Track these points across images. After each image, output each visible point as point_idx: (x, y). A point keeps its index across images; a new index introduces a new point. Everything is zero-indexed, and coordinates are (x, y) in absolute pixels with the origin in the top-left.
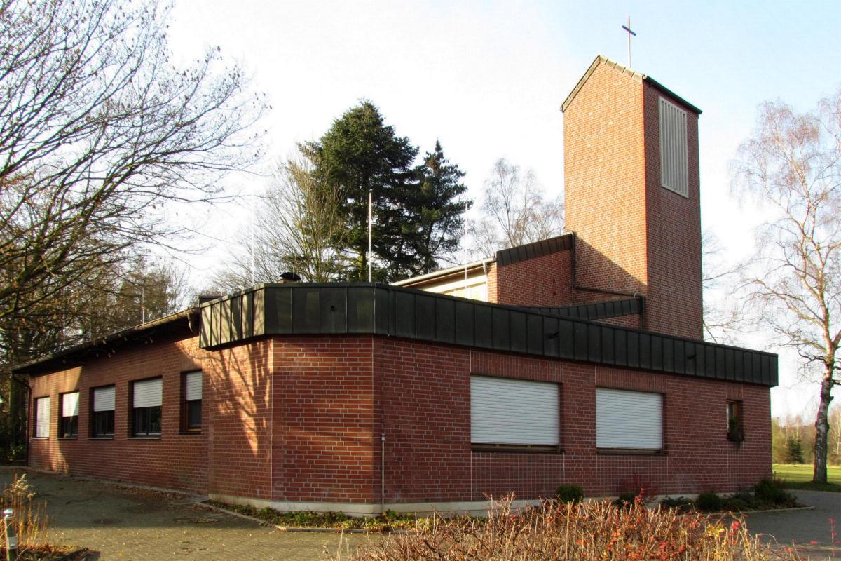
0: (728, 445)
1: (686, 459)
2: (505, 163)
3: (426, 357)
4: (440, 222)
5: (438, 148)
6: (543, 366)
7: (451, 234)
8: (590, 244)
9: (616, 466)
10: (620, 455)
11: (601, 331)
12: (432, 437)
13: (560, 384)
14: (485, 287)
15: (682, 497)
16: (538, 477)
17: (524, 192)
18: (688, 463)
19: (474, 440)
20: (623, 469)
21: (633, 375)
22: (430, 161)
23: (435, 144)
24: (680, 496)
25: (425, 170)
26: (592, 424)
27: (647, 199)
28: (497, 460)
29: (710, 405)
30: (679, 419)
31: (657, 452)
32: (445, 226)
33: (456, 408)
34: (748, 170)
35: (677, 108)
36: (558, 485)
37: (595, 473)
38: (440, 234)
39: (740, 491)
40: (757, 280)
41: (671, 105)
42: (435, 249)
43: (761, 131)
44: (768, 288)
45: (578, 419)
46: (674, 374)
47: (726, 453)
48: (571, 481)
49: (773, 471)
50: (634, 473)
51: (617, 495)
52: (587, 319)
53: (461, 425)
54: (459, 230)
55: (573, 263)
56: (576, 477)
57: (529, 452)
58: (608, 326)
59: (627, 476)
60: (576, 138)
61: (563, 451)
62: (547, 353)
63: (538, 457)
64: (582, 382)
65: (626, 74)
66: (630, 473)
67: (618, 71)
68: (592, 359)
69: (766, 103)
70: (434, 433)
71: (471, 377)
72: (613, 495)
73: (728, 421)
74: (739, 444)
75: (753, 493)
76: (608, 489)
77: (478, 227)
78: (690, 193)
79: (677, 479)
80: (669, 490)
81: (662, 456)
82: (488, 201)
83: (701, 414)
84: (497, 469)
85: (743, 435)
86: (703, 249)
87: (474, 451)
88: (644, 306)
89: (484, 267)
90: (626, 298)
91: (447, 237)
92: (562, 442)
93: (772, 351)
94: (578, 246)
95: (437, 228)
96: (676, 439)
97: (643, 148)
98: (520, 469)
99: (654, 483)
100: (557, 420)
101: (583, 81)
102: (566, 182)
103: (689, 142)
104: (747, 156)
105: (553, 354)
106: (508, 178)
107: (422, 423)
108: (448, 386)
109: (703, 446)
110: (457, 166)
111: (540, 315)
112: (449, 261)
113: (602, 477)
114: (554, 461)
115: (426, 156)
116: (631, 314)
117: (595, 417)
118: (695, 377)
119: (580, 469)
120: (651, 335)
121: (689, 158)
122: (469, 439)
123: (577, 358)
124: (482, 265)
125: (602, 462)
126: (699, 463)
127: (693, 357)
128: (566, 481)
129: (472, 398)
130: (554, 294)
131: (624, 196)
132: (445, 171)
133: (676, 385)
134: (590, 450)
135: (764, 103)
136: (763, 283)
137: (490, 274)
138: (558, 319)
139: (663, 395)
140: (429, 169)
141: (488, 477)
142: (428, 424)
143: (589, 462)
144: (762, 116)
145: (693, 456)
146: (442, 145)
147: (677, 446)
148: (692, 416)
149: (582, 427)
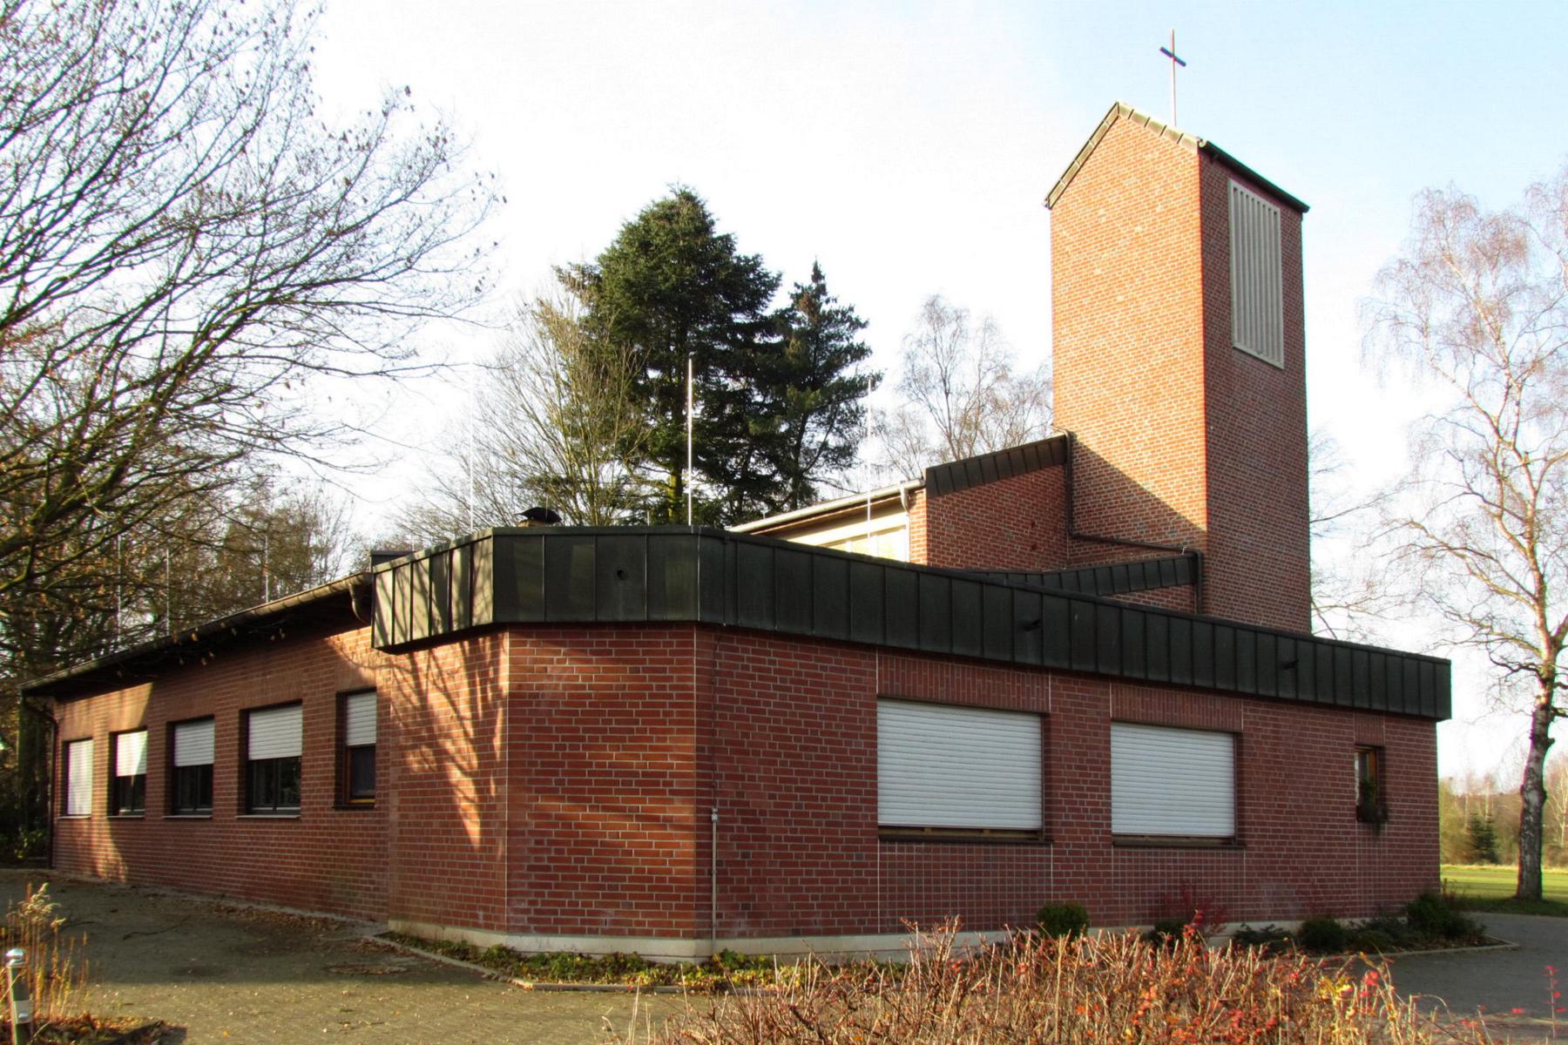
0: (1357, 829)
1: (1280, 856)
5: (817, 275)
7: (842, 435)
8: (1101, 454)
9: (1149, 868)
12: (806, 814)
13: (1044, 716)
14: (903, 536)
15: (1272, 926)
17: (977, 358)
20: (1163, 874)
21: (1179, 699)
25: (793, 317)
28: (927, 858)
30: (1267, 780)
31: (1226, 842)
32: (830, 422)
34: (1395, 317)
35: (1263, 201)
37: (1109, 881)
40: (1412, 522)
41: (1252, 195)
43: (1419, 245)
44: (1433, 537)
45: (1078, 781)
46: (1256, 698)
47: (1354, 845)
48: (1063, 896)
49: (1442, 877)
51: (1150, 923)
53: (859, 793)
54: (855, 429)
55: (1069, 489)
57: (987, 842)
58: (1134, 608)
59: (1169, 887)
60: (1075, 257)
61: (1049, 841)
62: (1019, 659)
63: (1002, 851)
66: (1175, 881)
72: (1144, 923)
73: (1357, 784)
74: (1379, 828)
75: (1403, 919)
77: (892, 422)
80: (1248, 912)
81: (1236, 849)
82: (910, 375)
87: (883, 839)
89: (903, 497)
90: (1168, 555)
91: (833, 441)
92: (1048, 823)
93: (1440, 654)
94: (1077, 460)
97: (1199, 276)
99: (1219, 900)
102: (1057, 338)
103: (1285, 264)
104: (1392, 291)
108: (834, 718)
109: (1311, 832)
110: (851, 309)
112: (837, 486)
113: (1123, 888)
114: (1034, 859)
115: (794, 290)
116: (1177, 585)
118: (1297, 703)
119: (1083, 874)
120: (1215, 624)
121: (1286, 295)
122: (875, 817)
123: (1075, 667)
124: (898, 494)
127: (1293, 665)
128: (1056, 896)
130: (1034, 548)
132: (829, 318)
134: (1101, 839)
136: (1423, 528)
137: (914, 510)
139: (1237, 737)
140: (800, 314)
142: (798, 789)
147: (1262, 830)
149: (1086, 796)
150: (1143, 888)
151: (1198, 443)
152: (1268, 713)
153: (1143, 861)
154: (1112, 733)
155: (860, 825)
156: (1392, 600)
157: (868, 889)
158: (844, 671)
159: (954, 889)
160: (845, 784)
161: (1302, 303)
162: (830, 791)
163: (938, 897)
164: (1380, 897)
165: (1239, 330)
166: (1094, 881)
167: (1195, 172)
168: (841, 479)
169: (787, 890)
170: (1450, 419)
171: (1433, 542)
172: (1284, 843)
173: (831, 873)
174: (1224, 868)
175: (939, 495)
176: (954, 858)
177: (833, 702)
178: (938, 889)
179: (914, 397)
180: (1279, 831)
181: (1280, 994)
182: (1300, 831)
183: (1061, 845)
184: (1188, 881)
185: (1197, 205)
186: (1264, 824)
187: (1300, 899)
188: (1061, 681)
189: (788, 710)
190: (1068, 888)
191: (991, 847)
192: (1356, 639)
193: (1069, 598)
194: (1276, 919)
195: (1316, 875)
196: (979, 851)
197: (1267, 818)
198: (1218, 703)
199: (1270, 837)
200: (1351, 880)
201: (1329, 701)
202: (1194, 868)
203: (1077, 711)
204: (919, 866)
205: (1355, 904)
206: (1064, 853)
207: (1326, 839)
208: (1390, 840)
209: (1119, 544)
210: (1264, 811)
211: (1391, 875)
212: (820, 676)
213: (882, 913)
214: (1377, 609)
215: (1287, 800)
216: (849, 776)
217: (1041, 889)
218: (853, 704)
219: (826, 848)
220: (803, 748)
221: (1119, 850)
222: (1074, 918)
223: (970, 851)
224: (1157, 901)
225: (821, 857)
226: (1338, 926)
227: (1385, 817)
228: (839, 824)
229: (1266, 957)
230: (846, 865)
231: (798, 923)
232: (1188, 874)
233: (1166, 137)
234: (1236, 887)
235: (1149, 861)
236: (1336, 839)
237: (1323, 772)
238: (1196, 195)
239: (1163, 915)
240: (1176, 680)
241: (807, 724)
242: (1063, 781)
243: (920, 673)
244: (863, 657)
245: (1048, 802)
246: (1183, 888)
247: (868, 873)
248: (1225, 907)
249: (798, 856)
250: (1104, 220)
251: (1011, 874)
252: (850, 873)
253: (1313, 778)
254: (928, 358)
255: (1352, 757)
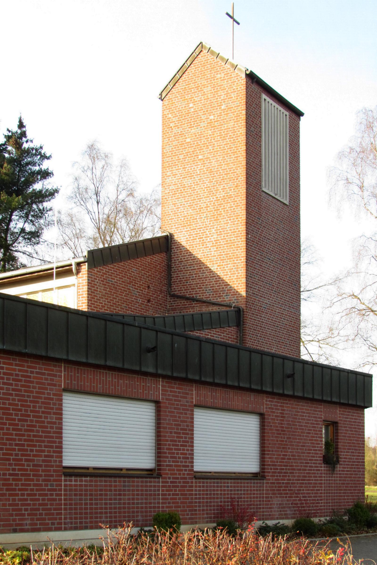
0: (323, 468)
1: (283, 483)
2: (98, 146)
3: (15, 370)
4: (21, 211)
5: (21, 125)
6: (81, 374)
7: (34, 224)
8: (188, 247)
9: (214, 490)
10: (217, 479)
11: (200, 344)
12: (21, 460)
13: (157, 403)
14: (73, 290)
15: (279, 523)
16: (133, 503)
17: (117, 182)
18: (285, 487)
19: (66, 463)
20: (221, 494)
21: (231, 394)
22: (11, 140)
23: (18, 120)
24: (277, 521)
25: (5, 149)
26: (190, 446)
27: (247, 203)
28: (91, 486)
29: (307, 426)
30: (277, 441)
31: (255, 476)
32: (27, 216)
33: (47, 427)
34: (347, 179)
35: (280, 108)
36: (154, 511)
37: (192, 499)
38: (20, 225)
39: (335, 516)
40: (353, 295)
41: (274, 104)
42: (14, 241)
43: (359, 140)
44: (364, 304)
45: (175, 441)
46: (272, 394)
47: (322, 477)
48: (167, 507)
49: (366, 494)
50: (231, 498)
51: (214, 522)
52: (174, 330)
53: (52, 447)
54: (42, 221)
55: (169, 267)
56: (173, 503)
57: (124, 476)
58: (208, 341)
59: (225, 502)
60: (175, 130)
61: (159, 475)
62: (144, 369)
63: (133, 482)
64: (180, 401)
65: (229, 67)
66: (228, 498)
67: (220, 62)
68: (190, 376)
69: (365, 110)
70: (22, 455)
71: (64, 394)
72: (211, 522)
73: (323, 443)
74: (334, 467)
75: (346, 518)
76: (205, 516)
77: (65, 219)
78: (290, 199)
79: (274, 504)
80: (266, 515)
81: (260, 479)
82: (76, 190)
83: (298, 436)
84: (91, 495)
85: (338, 458)
86: (302, 259)
87: (66, 475)
88: (242, 319)
89: (74, 267)
90: (224, 309)
91: (29, 228)
92: (159, 465)
93: (365, 370)
94: (174, 250)
95: (17, 217)
96: (274, 462)
97: (244, 148)
98: (115, 495)
99: (251, 509)
100: (154, 441)
101: (184, 69)
102: (164, 176)
103: (290, 145)
104: (346, 164)
105: (151, 370)
106: (99, 164)
107: (11, 444)
108: (38, 402)
109: (300, 470)
110: (41, 148)
111: (138, 327)
112: (30, 255)
113: (200, 502)
114: (151, 486)
115: (7, 133)
116: (229, 327)
117: (193, 438)
118: (293, 397)
119: (178, 495)
120: (251, 351)
121: (290, 163)
122: (61, 462)
123: (175, 375)
124: (71, 265)
125: (200, 487)
126: (296, 487)
127: (292, 376)
128: (163, 507)
129: (64, 416)
130: (149, 301)
131: (224, 198)
132: (28, 152)
133: (275, 405)
134: (188, 474)
135: (364, 111)
136: (359, 298)
137: (80, 275)
138: (157, 331)
139: (262, 416)
140: (10, 148)
141: (81, 504)
142: (16, 445)
143: (186, 487)
144: (361, 123)
145: (290, 480)
146: (25, 123)
147: (274, 469)
148: (290, 438)
149: (180, 450)
150: (211, 502)
151: (243, 244)
152: (279, 403)
153: (211, 487)
154: (195, 413)
155: (52, 466)
156: (342, 338)
157: (57, 504)
158: (44, 374)
159: (106, 504)
160: (44, 442)
161: (299, 168)
162: (35, 446)
163: (96, 509)
164: (334, 506)
165: (265, 181)
166: (183, 499)
167: (244, 88)
168: (32, 251)
169: (10, 505)
170: (373, 238)
171: (364, 307)
172: (286, 476)
173: (35, 495)
174: (254, 490)
175: (95, 267)
176: (106, 486)
177: (37, 393)
178: (96, 504)
179: (78, 204)
180: (283, 469)
181: (297, 561)
182: (294, 469)
183: (165, 478)
184: (234, 498)
185: (244, 107)
186: (276, 465)
187: (294, 507)
188: (166, 382)
189: (11, 397)
190: (169, 503)
191: (126, 479)
192: (323, 361)
193: (172, 334)
194: (283, 519)
195: (302, 494)
196: (120, 482)
197: (277, 462)
198: (252, 397)
199: (279, 473)
200: (319, 497)
201: (311, 396)
202: (238, 490)
203: (175, 400)
204: (86, 490)
205: (322, 509)
206: (167, 482)
207: (307, 473)
208: (340, 474)
209: (197, 301)
210: (276, 458)
211: (340, 493)
212: (30, 377)
213: (65, 518)
214: (334, 343)
215: (287, 452)
216: (46, 437)
217: (154, 503)
218: (49, 394)
219: (33, 480)
220: (19, 420)
221: (198, 480)
222: (173, 520)
223: (115, 482)
224: (217, 510)
225: (29, 485)
226: (313, 522)
227: (338, 461)
228: (41, 466)
229: (288, 540)
230: (44, 490)
231: (17, 525)
232: (235, 494)
233: (228, 66)
234: (260, 501)
235: (214, 486)
236: (313, 473)
237: (306, 436)
238: (244, 101)
239: (221, 517)
240: (229, 383)
241: (22, 405)
242: (167, 441)
243: (81, 375)
244: (55, 366)
245: (159, 453)
246: (232, 502)
247: (57, 495)
248: (254, 512)
249: (16, 485)
250: (192, 110)
251: (138, 495)
252: (46, 495)
253: (301, 439)
254: (87, 179)
255: (322, 428)
